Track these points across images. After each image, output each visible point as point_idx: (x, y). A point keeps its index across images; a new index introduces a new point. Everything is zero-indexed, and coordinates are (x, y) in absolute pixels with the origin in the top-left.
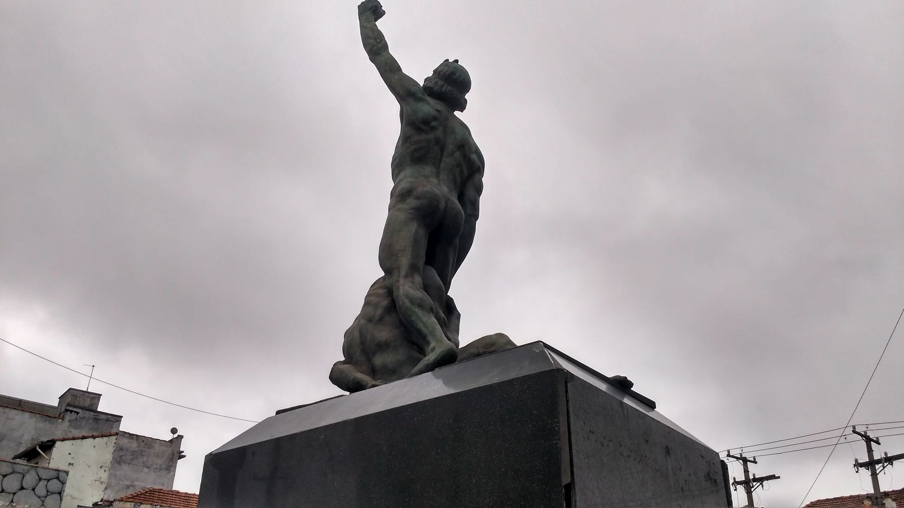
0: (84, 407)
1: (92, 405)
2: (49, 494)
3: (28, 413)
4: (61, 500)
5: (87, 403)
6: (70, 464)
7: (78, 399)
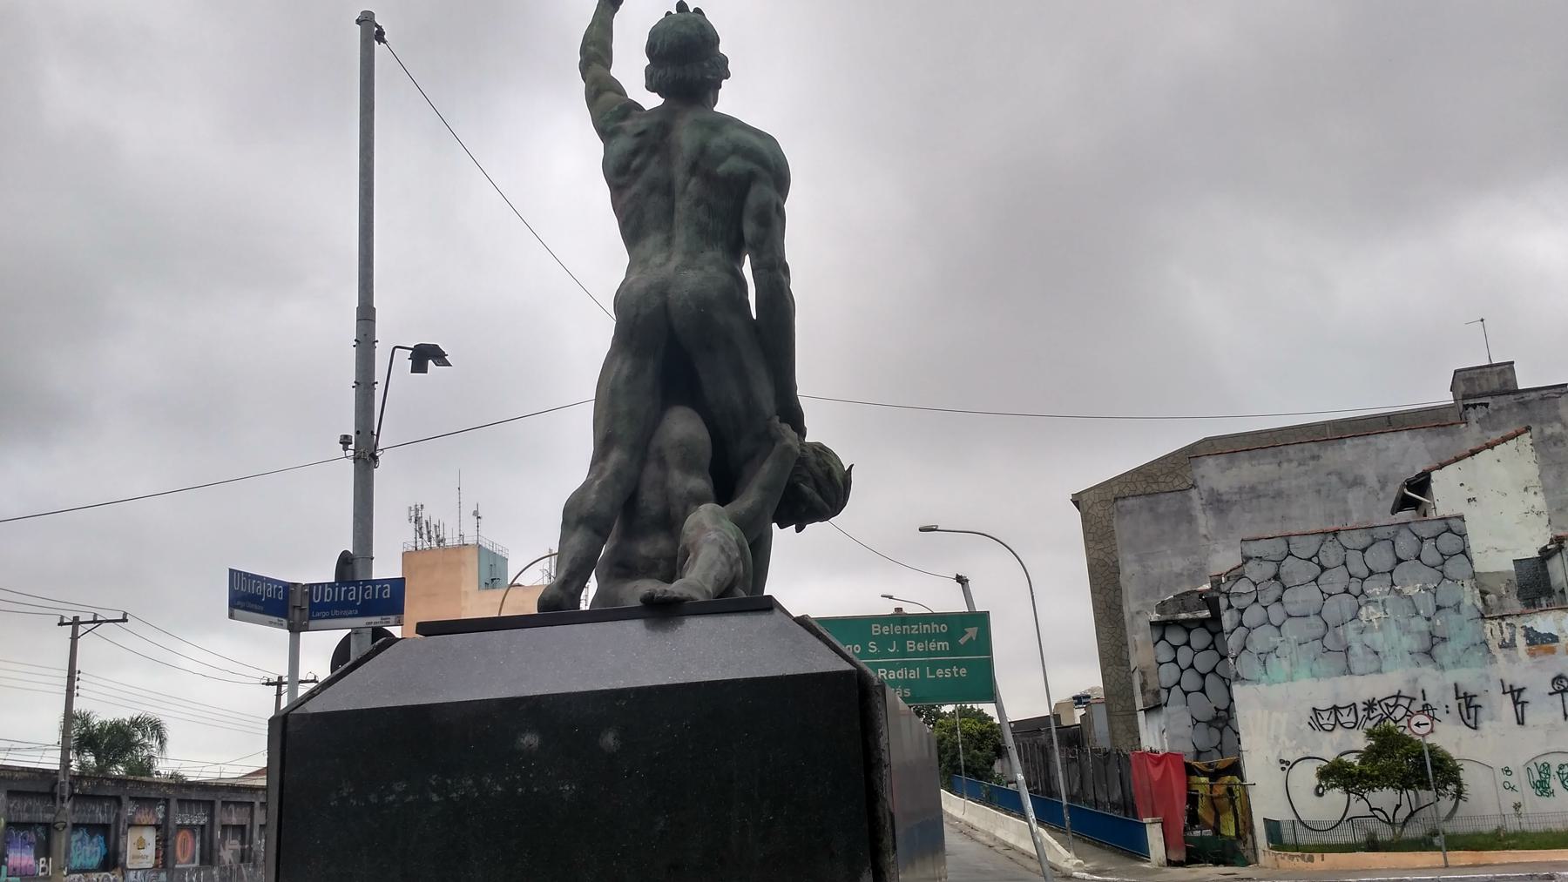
0: (1493, 392)
1: (1505, 383)
2: (1446, 557)
3: (1406, 432)
4: (1471, 562)
5: (1495, 383)
6: (1469, 500)
7: (1477, 383)
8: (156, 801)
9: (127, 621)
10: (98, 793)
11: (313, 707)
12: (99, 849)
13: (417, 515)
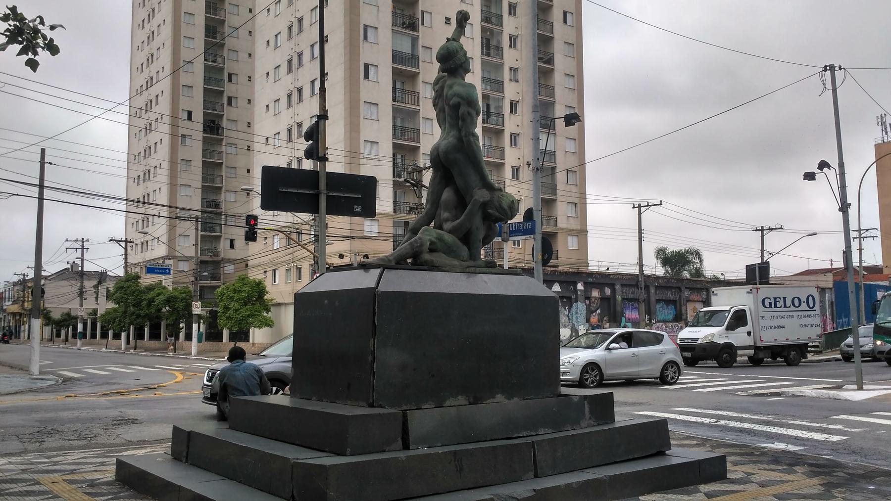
8: (700, 290)
9: (662, 204)
10: (668, 285)
11: (299, 292)
12: (672, 311)
13: (882, 120)
